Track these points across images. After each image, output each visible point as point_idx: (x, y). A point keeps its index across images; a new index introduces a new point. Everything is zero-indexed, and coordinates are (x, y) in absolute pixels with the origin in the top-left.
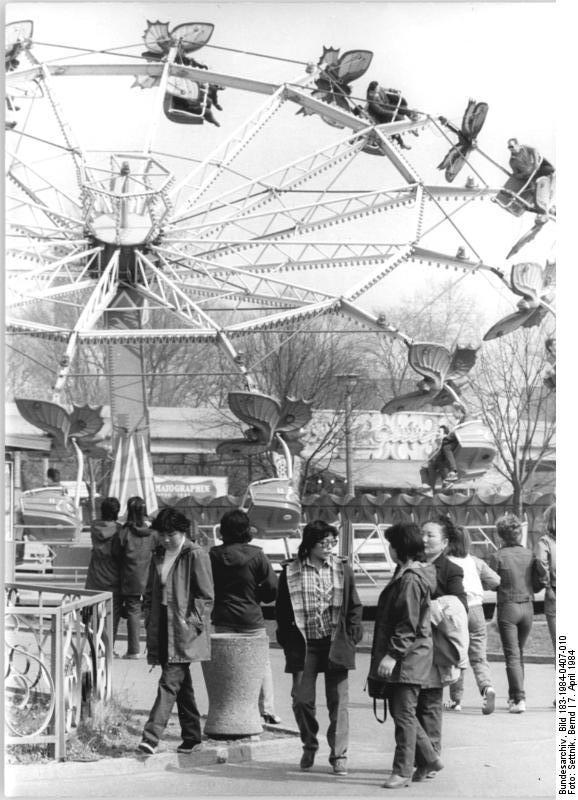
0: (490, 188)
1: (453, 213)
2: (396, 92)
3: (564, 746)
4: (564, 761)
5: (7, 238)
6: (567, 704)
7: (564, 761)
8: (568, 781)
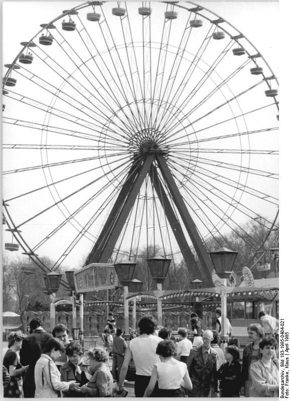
0: (263, 78)
1: (75, 71)
2: (58, 386)
3: (283, 374)
4: (283, 381)
6: (137, 131)
7: (283, 381)
8: (285, 391)
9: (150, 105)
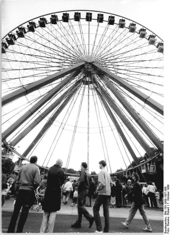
3: (166, 219)
4: (166, 224)
5: (97, 18)
7: (166, 224)
8: (167, 229)
9: (73, 46)
